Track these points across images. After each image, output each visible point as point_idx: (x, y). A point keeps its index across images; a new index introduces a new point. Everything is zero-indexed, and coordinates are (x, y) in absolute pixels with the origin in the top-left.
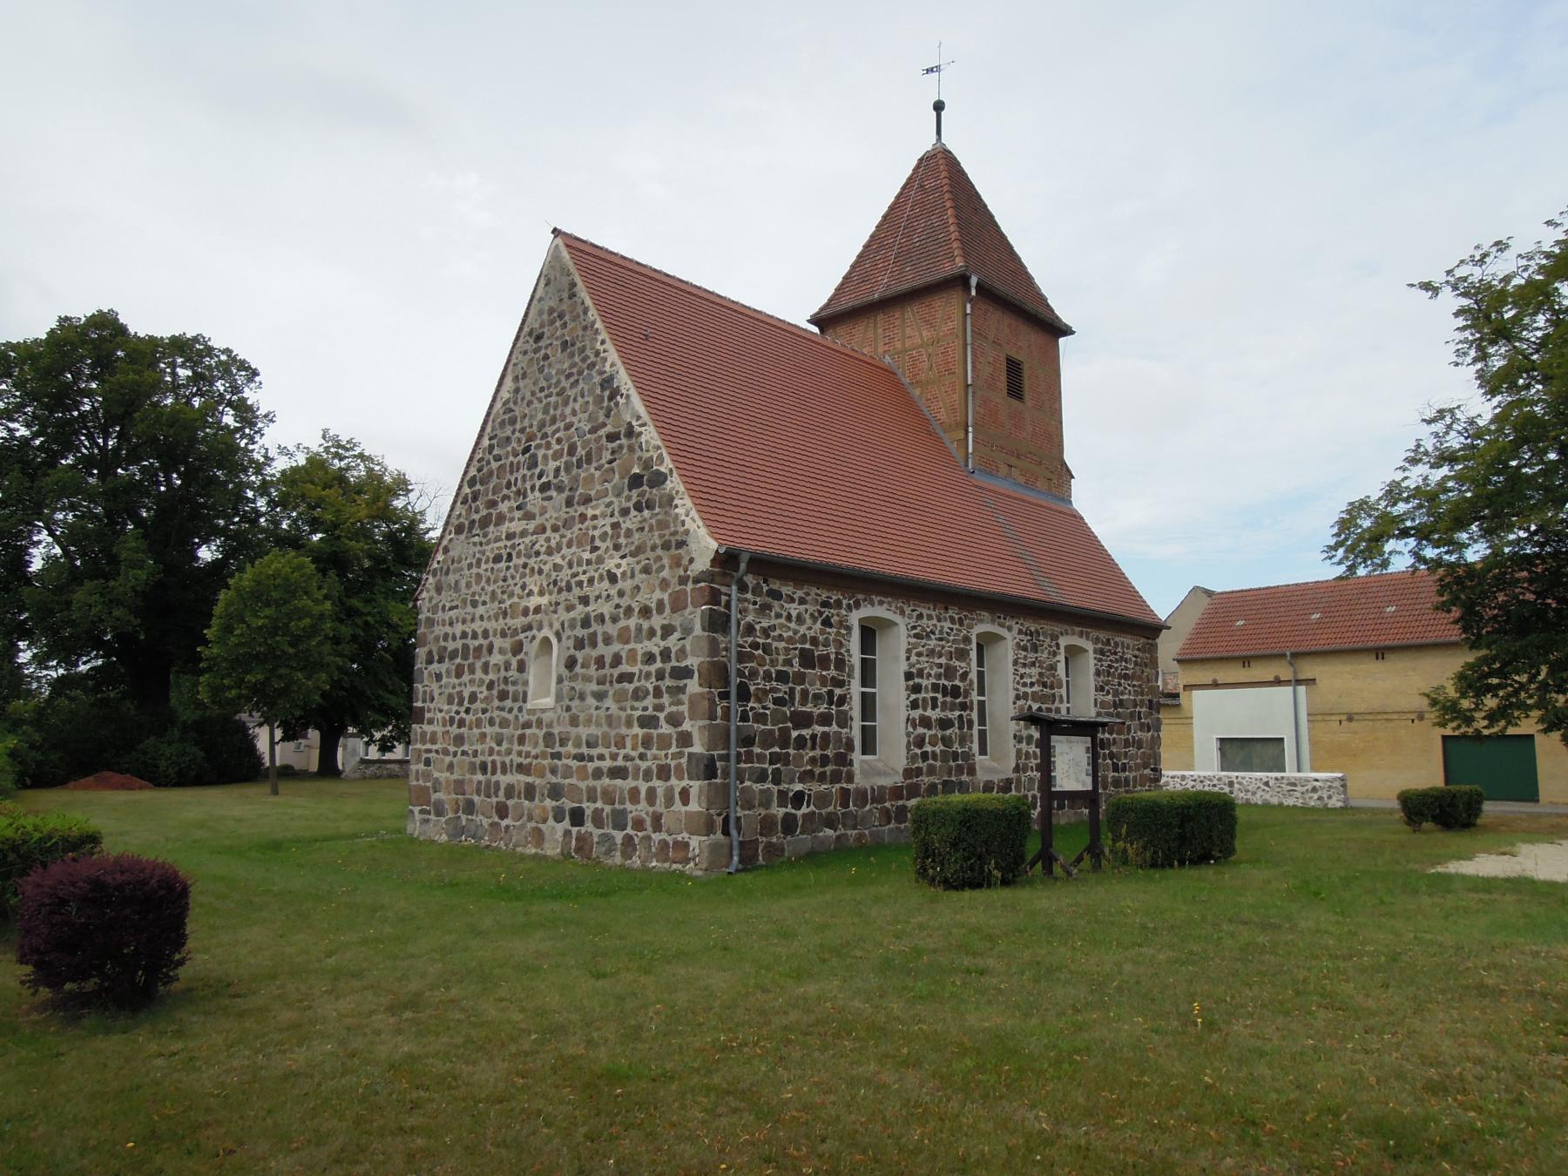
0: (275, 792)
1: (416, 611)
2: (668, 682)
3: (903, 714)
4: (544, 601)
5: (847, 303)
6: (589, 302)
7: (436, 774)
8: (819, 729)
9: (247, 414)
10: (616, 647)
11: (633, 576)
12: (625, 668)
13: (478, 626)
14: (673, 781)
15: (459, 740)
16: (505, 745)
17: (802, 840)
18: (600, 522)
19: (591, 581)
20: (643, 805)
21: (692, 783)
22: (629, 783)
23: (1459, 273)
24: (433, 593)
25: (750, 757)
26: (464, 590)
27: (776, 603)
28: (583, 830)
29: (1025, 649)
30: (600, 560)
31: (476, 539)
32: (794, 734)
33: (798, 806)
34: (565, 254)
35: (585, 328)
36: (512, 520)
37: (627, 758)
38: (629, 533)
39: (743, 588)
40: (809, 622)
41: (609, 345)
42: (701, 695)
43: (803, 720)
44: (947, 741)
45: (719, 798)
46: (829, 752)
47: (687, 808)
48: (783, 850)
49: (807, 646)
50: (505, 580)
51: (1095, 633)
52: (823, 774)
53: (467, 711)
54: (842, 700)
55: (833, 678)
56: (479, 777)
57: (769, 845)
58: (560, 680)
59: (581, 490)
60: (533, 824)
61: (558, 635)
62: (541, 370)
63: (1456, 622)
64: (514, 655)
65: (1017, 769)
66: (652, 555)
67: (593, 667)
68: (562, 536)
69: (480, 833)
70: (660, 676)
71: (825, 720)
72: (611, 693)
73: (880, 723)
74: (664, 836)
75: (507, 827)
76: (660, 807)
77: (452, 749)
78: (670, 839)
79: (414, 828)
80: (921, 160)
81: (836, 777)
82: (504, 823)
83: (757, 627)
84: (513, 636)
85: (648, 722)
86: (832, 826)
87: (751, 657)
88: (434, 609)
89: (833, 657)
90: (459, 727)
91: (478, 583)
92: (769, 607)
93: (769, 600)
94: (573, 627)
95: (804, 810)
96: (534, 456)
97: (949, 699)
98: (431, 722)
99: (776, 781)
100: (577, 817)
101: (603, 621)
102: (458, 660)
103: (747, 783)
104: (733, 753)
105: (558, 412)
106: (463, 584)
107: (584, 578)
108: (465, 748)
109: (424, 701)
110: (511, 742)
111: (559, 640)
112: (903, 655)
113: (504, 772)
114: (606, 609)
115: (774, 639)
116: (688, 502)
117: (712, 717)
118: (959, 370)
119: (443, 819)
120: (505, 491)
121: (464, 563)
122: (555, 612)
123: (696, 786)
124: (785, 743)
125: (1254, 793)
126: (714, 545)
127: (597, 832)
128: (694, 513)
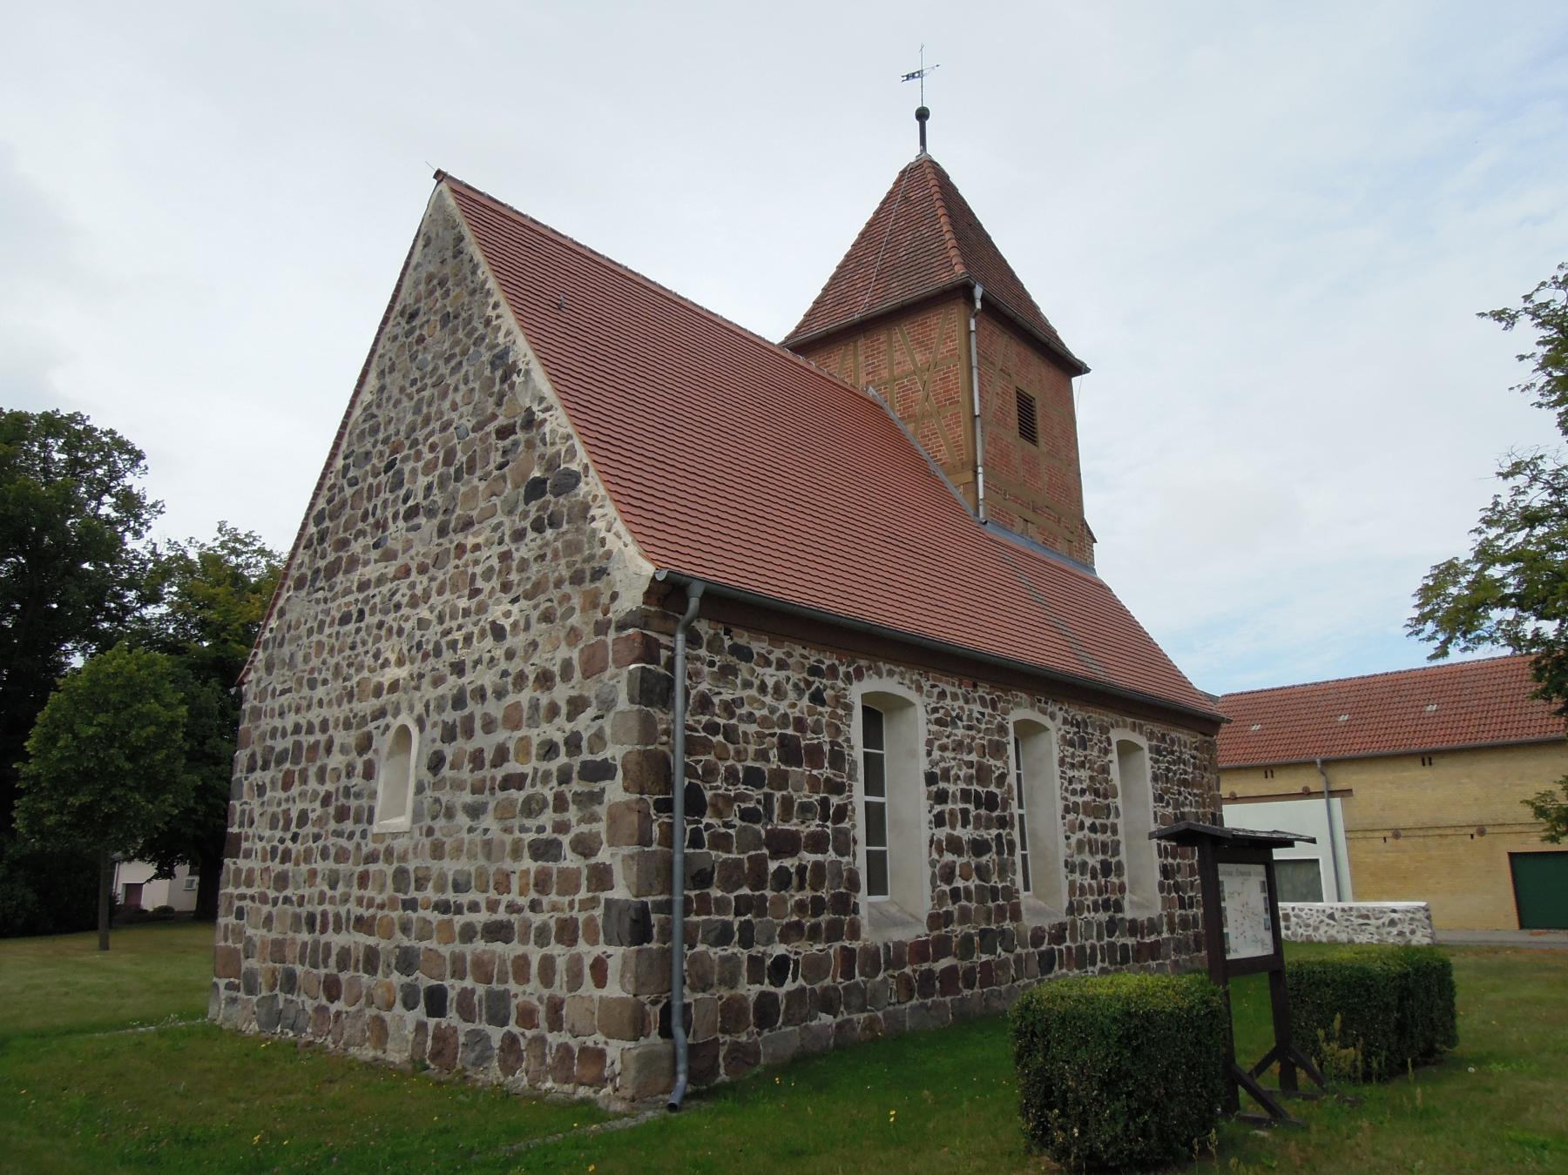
0: (104, 946)
1: (239, 698)
2: (577, 786)
3: (925, 832)
4: (402, 673)
5: (818, 329)
6: (479, 256)
7: (250, 932)
8: (809, 858)
9: (130, 503)
10: (501, 735)
11: (527, 627)
12: (512, 767)
13: (315, 716)
14: (582, 946)
15: (282, 881)
16: (341, 888)
17: (785, 1037)
18: (485, 553)
19: (468, 639)
20: (535, 983)
21: (610, 950)
22: (513, 949)
23: (1539, 298)
24: (262, 672)
25: (704, 905)
26: (301, 666)
27: (743, 666)
28: (444, 1022)
29: (1071, 744)
30: (482, 608)
31: (320, 595)
32: (773, 866)
33: (779, 980)
34: (451, 201)
35: (473, 293)
36: (366, 563)
37: (512, 908)
38: (524, 565)
39: (693, 640)
40: (792, 695)
41: (505, 309)
42: (627, 805)
43: (784, 844)
44: (983, 872)
45: (657, 974)
46: (824, 893)
47: (604, 992)
48: (757, 1054)
49: (790, 731)
50: (353, 648)
51: (1148, 727)
52: (815, 929)
53: (294, 838)
54: (842, 813)
55: (828, 780)
56: (305, 936)
57: (736, 1047)
58: (420, 789)
59: (459, 512)
60: (373, 1011)
61: (420, 722)
62: (413, 358)
63: (1559, 713)
64: (360, 754)
65: (1071, 910)
66: (555, 594)
67: (467, 767)
68: (432, 579)
69: (301, 1022)
70: (564, 777)
71: (817, 843)
72: (491, 807)
73: (892, 846)
74: (564, 1037)
75: (338, 1014)
76: (559, 989)
77: (272, 894)
78: (575, 1044)
79: (218, 1011)
80: (903, 173)
81: (834, 932)
82: (334, 1007)
83: (716, 700)
84: (359, 726)
85: (545, 850)
86: (830, 1009)
87: (707, 747)
88: (261, 695)
89: (827, 748)
90: (283, 861)
91: (318, 655)
92: (734, 671)
93: (733, 660)
94: (440, 708)
95: (789, 986)
96: (400, 472)
97: (980, 809)
98: (248, 854)
99: (746, 942)
100: (436, 1002)
101: (483, 697)
102: (287, 765)
103: (701, 948)
104: (678, 899)
105: (434, 409)
106: (300, 657)
107: (458, 636)
108: (288, 892)
109: (241, 825)
110: (349, 884)
111: (422, 729)
112: (923, 749)
113: (338, 929)
114: (488, 679)
115: (741, 719)
116: (611, 510)
117: (644, 840)
118: (962, 398)
119: (255, 999)
120: (360, 525)
121: (303, 629)
122: (417, 688)
123: (617, 955)
124: (758, 881)
125: (1316, 929)
126: (648, 569)
127: (464, 1027)
128: (619, 526)
